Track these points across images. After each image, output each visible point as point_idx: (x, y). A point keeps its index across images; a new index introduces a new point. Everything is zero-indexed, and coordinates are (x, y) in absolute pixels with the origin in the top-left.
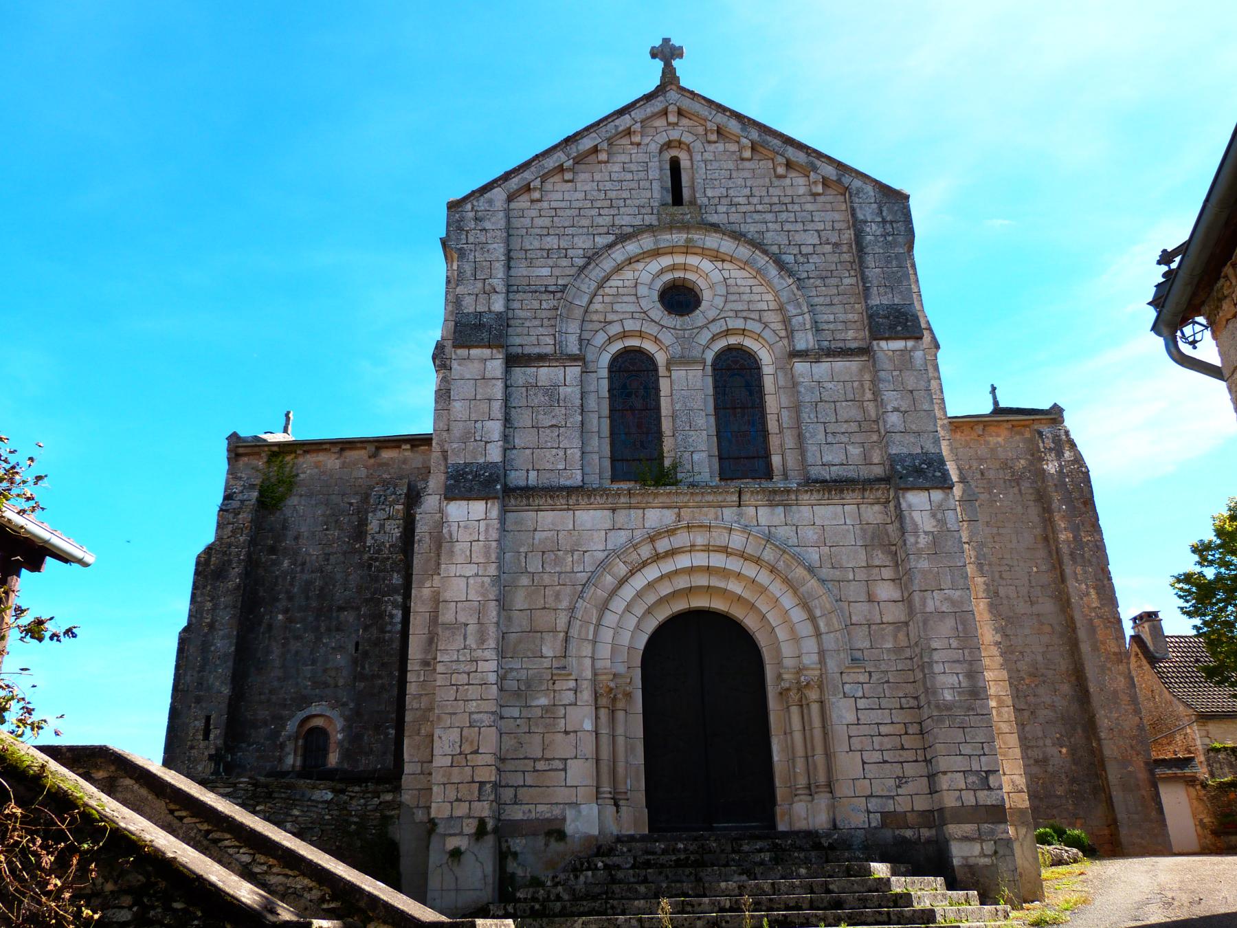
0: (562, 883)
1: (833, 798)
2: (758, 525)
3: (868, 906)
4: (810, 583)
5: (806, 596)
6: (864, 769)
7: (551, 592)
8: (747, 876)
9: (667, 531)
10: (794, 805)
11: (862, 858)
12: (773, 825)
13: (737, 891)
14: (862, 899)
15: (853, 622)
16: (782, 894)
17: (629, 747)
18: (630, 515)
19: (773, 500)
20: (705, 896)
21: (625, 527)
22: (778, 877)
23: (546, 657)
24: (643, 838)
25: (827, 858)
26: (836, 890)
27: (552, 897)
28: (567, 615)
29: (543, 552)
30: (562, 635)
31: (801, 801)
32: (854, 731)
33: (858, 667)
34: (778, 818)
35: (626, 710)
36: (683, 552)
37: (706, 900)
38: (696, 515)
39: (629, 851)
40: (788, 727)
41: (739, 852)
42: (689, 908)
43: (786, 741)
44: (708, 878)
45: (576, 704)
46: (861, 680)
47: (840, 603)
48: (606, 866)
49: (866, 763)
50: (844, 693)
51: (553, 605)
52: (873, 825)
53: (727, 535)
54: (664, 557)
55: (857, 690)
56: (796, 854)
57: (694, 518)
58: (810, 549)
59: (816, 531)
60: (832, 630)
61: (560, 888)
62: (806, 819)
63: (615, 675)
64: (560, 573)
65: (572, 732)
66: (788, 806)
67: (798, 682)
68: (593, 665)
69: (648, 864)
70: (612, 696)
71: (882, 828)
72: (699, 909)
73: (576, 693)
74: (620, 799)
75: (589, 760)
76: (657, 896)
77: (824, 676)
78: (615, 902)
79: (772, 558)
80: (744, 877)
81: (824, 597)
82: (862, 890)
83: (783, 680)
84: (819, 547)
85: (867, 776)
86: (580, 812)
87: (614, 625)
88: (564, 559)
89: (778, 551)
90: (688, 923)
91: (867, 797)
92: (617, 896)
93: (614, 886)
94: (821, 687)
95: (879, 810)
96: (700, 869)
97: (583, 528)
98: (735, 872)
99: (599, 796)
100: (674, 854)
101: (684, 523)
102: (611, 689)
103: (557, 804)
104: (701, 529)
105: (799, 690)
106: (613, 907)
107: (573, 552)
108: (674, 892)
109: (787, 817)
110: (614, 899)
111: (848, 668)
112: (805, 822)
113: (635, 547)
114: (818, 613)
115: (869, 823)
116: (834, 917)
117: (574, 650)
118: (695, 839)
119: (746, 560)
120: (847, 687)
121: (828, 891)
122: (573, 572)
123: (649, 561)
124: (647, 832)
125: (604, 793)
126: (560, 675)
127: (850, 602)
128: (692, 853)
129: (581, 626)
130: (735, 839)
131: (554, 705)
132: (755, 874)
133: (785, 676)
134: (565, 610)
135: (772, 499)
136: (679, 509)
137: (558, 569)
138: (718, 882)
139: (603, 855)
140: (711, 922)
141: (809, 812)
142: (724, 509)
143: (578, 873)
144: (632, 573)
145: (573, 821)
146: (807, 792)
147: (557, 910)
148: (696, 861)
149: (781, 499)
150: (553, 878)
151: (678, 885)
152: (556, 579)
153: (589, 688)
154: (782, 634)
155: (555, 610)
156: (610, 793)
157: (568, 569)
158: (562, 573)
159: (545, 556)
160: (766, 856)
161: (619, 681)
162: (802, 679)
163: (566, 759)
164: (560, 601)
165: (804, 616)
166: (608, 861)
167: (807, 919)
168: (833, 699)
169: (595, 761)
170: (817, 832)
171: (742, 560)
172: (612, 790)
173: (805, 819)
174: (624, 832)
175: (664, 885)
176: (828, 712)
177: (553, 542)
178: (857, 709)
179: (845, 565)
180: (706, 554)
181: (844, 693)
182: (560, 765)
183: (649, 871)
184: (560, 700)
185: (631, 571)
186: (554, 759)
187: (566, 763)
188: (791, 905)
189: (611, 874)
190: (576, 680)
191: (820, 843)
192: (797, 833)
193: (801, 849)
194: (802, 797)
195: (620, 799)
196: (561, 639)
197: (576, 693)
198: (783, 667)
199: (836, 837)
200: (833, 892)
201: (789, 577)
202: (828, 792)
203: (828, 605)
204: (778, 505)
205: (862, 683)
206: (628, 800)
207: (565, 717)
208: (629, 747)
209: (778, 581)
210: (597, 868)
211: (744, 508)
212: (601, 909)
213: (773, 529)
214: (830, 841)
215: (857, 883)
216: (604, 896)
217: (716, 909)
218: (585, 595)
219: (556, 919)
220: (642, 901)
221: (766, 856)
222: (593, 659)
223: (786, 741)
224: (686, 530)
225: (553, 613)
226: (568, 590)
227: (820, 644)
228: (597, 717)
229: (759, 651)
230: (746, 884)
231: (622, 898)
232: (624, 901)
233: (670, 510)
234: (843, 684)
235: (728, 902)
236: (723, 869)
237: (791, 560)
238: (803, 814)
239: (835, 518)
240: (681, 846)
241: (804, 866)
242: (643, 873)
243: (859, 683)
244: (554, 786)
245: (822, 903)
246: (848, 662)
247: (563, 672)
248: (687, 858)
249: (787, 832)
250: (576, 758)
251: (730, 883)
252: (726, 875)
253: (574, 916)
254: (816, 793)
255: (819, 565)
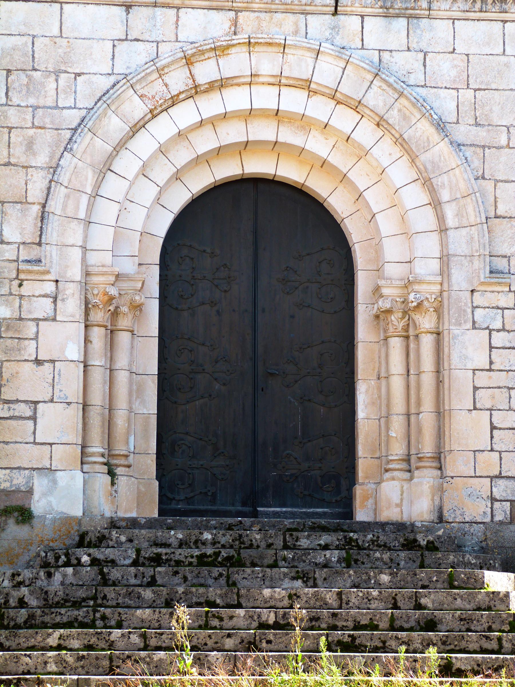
0: (27, 582)
1: (442, 477)
2: (363, 48)
3: (473, 628)
4: (437, 148)
5: (429, 167)
6: (492, 437)
7: (20, 139)
8: (304, 582)
9: (215, 49)
10: (383, 484)
11: (475, 565)
12: (349, 514)
13: (286, 602)
14: (465, 619)
15: (499, 213)
16: (351, 608)
17: (135, 387)
18: (154, 17)
19: (392, 7)
20: (239, 606)
21: (146, 37)
22: (348, 585)
23: (8, 243)
24: (150, 524)
25: (422, 561)
26: (430, 605)
27: (13, 602)
28: (45, 178)
29: (9, 71)
30: (36, 209)
31: (393, 479)
32: (482, 380)
33: (499, 284)
34: (358, 503)
35: (132, 331)
36: (238, 85)
37: (241, 612)
38: (264, 24)
39: (130, 541)
40: (383, 370)
41: (294, 547)
42: (215, 622)
43: (379, 389)
44: (245, 583)
45: (54, 319)
46: (502, 304)
47: (481, 181)
48: (94, 562)
49: (178, 10)
50: (474, 322)
51: (23, 160)
52: (498, 517)
53: (310, 62)
54: (206, 91)
55: (494, 319)
56: (378, 555)
57: (259, 27)
58: (443, 93)
59: (455, 62)
60: (465, 223)
61: (24, 590)
62: (399, 505)
63: (118, 276)
64: (36, 108)
65: (47, 361)
66: (373, 486)
67: (405, 302)
68: (84, 259)
69: (157, 560)
70: (112, 308)
71: (510, 523)
72: (231, 624)
73: (55, 302)
74: (117, 466)
75: (73, 405)
76: (169, 604)
77: (445, 294)
78: (108, 611)
79: (381, 104)
80: (299, 583)
81: (457, 171)
82: (468, 607)
83: (381, 296)
84: (457, 89)
85: (495, 447)
86: (55, 482)
87: (120, 198)
88: (42, 84)
89: (391, 92)
90: (213, 641)
91: (492, 478)
92: (110, 603)
93: (106, 590)
94: (438, 311)
95: (509, 498)
96: (236, 569)
97: (76, 35)
98: (285, 575)
99: (86, 459)
100: (197, 547)
101: (242, 37)
102: (111, 299)
103: (19, 468)
104: (270, 49)
105: (405, 313)
106: (104, 618)
107: (57, 73)
108: (195, 600)
109: (371, 501)
110: (106, 607)
111: (482, 284)
112: (397, 510)
113: (161, 72)
114: (445, 195)
115: (492, 516)
116: (423, 640)
117: (55, 234)
118: (230, 528)
119: (338, 103)
120: (479, 313)
121: (419, 607)
122: (57, 107)
123: (182, 96)
124: (156, 515)
125: (93, 455)
126: (30, 272)
127: (497, 181)
128: (223, 546)
129: (67, 196)
130: (289, 530)
131: (21, 319)
132: (315, 579)
133: (385, 291)
134: (42, 168)
135: (389, 4)
136: (237, 12)
137: (32, 101)
138: (260, 588)
139: (90, 545)
140: (246, 641)
141: (405, 495)
142: (309, 17)
143: (52, 570)
144: (153, 114)
145: (44, 495)
146: (404, 466)
147: (20, 620)
148: (229, 558)
149: (404, 6)
150: (13, 575)
151: (202, 590)
152: (29, 117)
153: (77, 296)
154: (268, 40)
155: (27, 167)
156: (103, 455)
157: (50, 102)
158: (38, 107)
159: (11, 78)
160: (334, 556)
161: (124, 285)
162: (411, 297)
163: (36, 403)
164: (34, 154)
165: (424, 198)
166: (98, 554)
167: (384, 642)
168: (456, 331)
169: (81, 406)
170: (413, 525)
171: (333, 103)
172: (106, 452)
173: (397, 505)
174: (121, 514)
175: (181, 590)
176: (446, 350)
177: (25, 55)
178: (491, 348)
179: (496, 121)
180: (275, 90)
181: (474, 322)
182: (26, 410)
183: (159, 569)
184: (30, 312)
185: (151, 111)
186: (17, 401)
187: (35, 409)
188: (363, 622)
189: (101, 573)
190: (57, 281)
191: (415, 540)
192: (383, 525)
193: (386, 547)
194: (396, 474)
195: (117, 466)
196: (34, 215)
197: (55, 302)
198: (382, 277)
199: (440, 533)
200: (425, 608)
201: (405, 136)
202: (436, 468)
203: (462, 185)
204: (398, 16)
205: (503, 309)
206: (129, 466)
207: (36, 338)
208: (135, 387)
209: (388, 140)
210: (79, 563)
211: (342, 17)
212: (86, 620)
213: (386, 56)
214: (431, 538)
215: (461, 597)
216: (92, 603)
217: (255, 624)
218: (75, 146)
219: (21, 631)
220: (148, 611)
221: (334, 556)
222: (84, 249)
223: (379, 389)
224: (245, 48)
225: (22, 172)
226: (48, 136)
227: (443, 244)
228: (87, 341)
229: (350, 249)
230: (301, 592)
231: (118, 605)
232: (120, 610)
233: (221, 13)
234: (474, 308)
235: (272, 615)
236: (268, 570)
237: (412, 109)
238: (396, 499)
239: (488, 44)
240: (207, 536)
241: (387, 571)
242: (149, 572)
243: (498, 308)
244: (16, 442)
245: (407, 622)
246: (484, 274)
247: (36, 268)
248: (217, 554)
249: (369, 523)
250: (52, 401)
251: (277, 590)
252: (272, 579)
253: (46, 627)
254: (417, 468)
255: (455, 120)
